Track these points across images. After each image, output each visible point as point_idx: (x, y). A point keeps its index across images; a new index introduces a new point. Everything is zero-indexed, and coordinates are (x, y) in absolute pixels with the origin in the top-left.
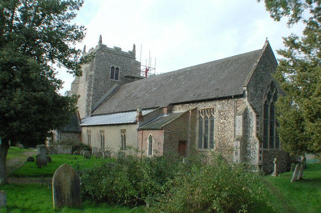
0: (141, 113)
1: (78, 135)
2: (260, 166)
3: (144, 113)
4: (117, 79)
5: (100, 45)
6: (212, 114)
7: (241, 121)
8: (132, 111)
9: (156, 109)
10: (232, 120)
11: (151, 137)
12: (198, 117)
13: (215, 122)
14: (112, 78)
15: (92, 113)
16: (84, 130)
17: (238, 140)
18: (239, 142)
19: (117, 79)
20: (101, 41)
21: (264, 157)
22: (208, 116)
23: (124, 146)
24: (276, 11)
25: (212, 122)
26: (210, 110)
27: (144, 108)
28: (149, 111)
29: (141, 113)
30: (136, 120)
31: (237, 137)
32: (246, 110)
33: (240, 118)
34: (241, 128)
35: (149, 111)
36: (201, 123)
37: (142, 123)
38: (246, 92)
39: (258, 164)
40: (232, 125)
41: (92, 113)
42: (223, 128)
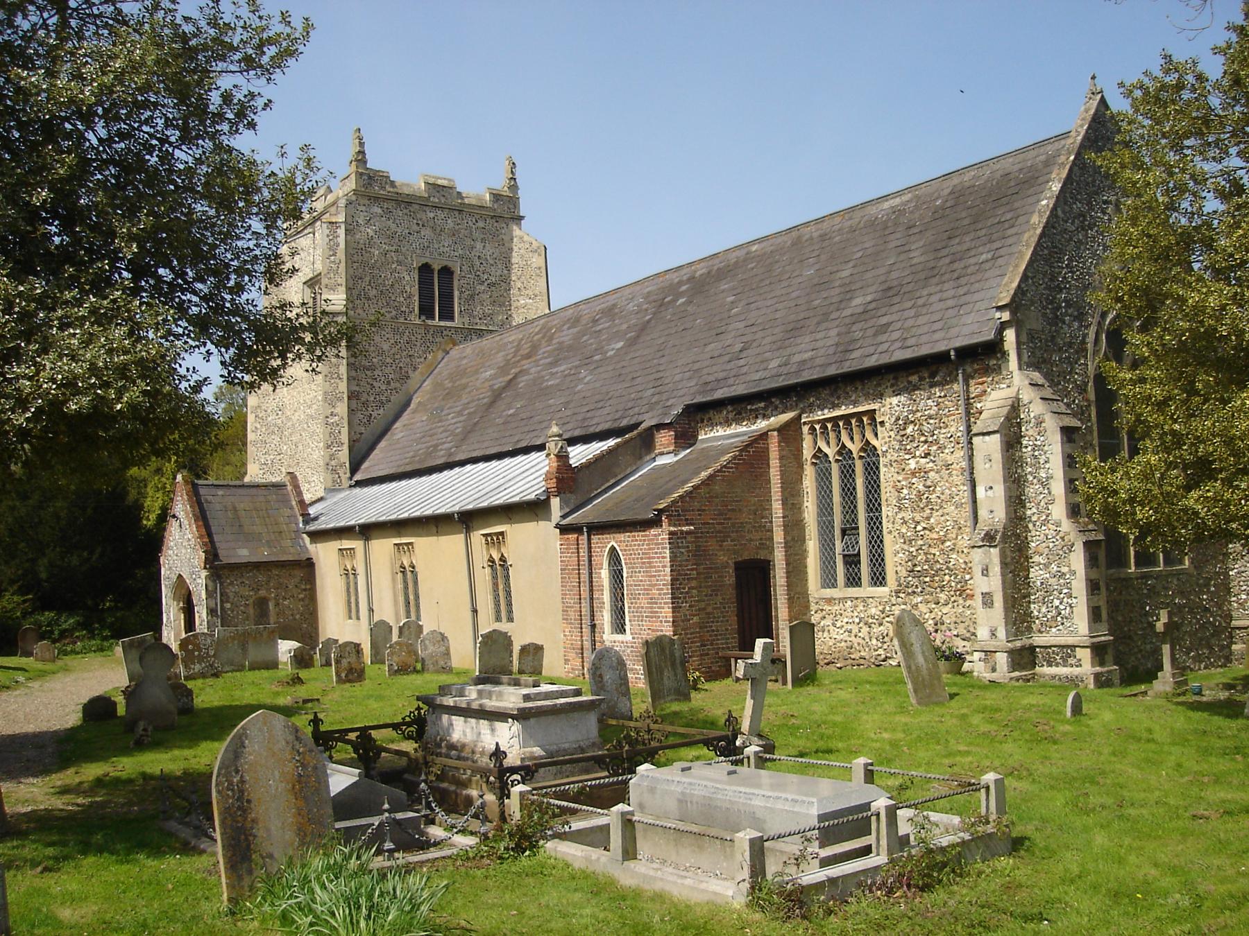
0: (563, 457)
1: (299, 573)
2: (1099, 651)
3: (579, 455)
4: (452, 318)
5: (359, 175)
6: (869, 435)
7: (997, 456)
8: (526, 450)
9: (611, 442)
10: (957, 457)
11: (614, 555)
12: (807, 452)
13: (883, 470)
14: (426, 311)
15: (354, 470)
16: (326, 556)
17: (989, 538)
18: (995, 552)
19: (452, 318)
20: (361, 157)
21: (1114, 606)
22: (854, 447)
23: (668, 594)
24: (219, 117)
25: (872, 470)
26: (824, 427)
27: (577, 433)
28: (598, 447)
29: (563, 457)
30: (547, 491)
31: (983, 527)
32: (1015, 407)
33: (990, 447)
34: (1000, 490)
35: (598, 447)
36: (823, 478)
37: (574, 500)
38: (1010, 335)
39: (1087, 641)
40: (958, 479)
41: (354, 470)
42: (920, 495)
